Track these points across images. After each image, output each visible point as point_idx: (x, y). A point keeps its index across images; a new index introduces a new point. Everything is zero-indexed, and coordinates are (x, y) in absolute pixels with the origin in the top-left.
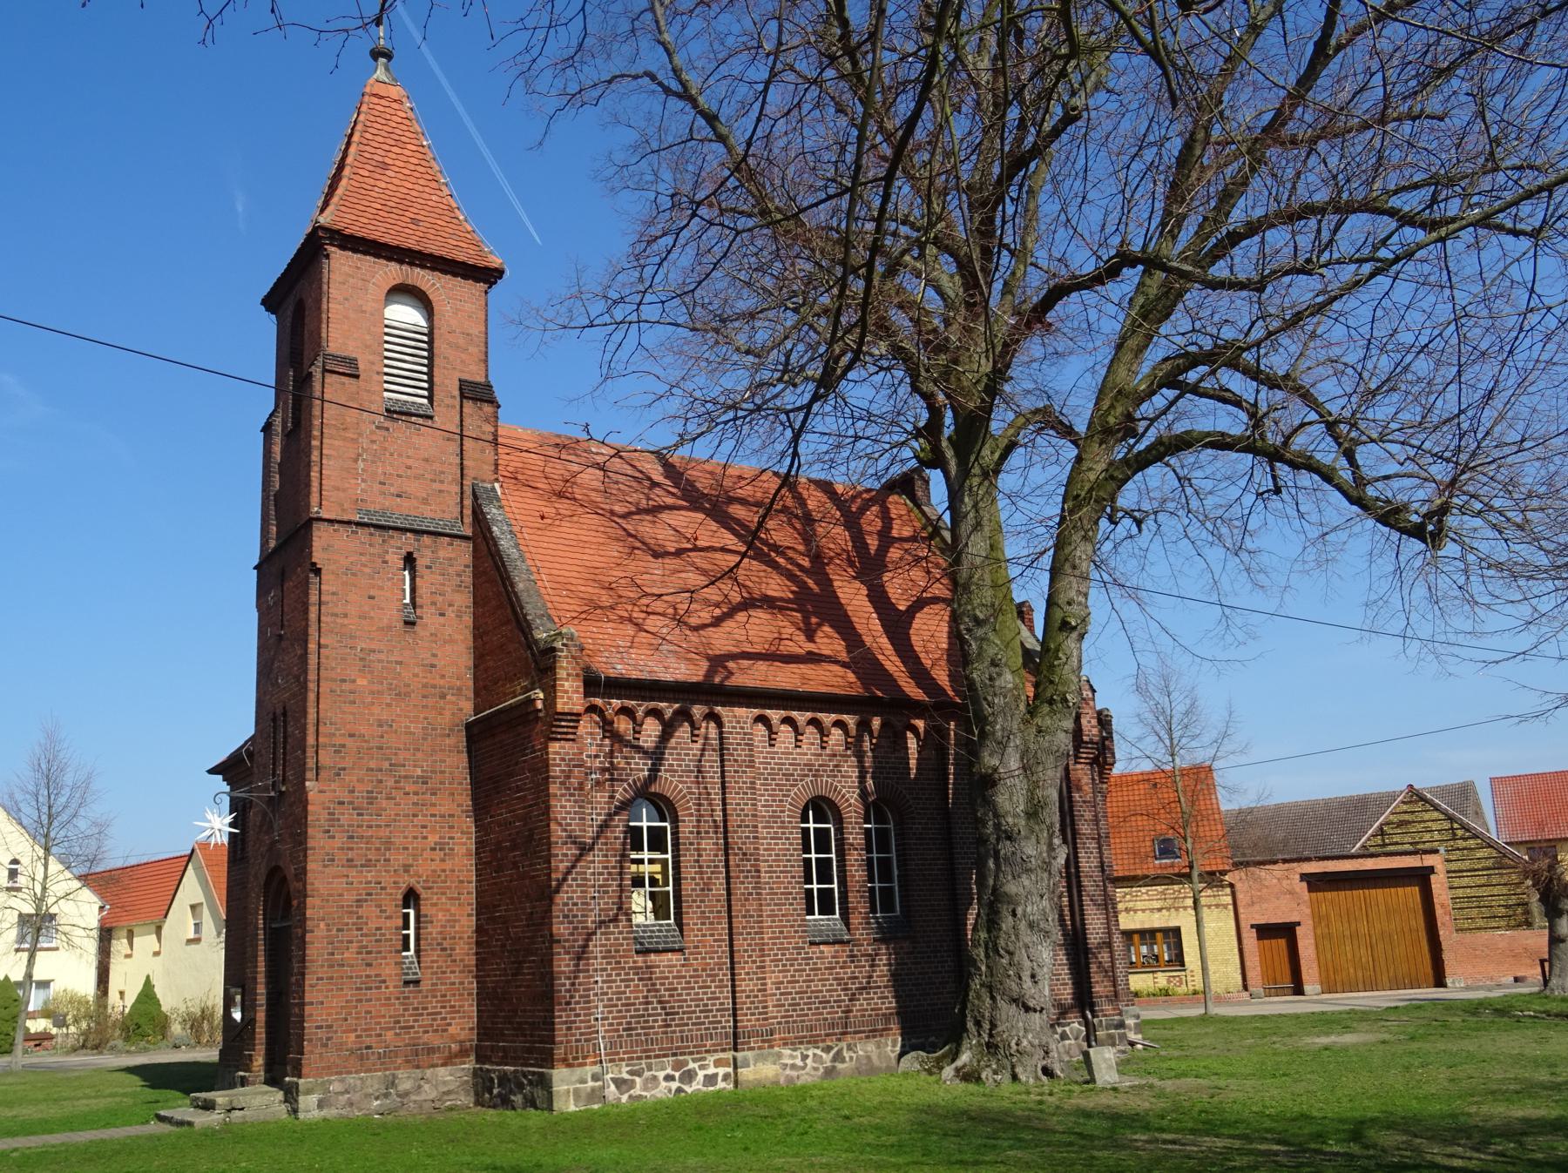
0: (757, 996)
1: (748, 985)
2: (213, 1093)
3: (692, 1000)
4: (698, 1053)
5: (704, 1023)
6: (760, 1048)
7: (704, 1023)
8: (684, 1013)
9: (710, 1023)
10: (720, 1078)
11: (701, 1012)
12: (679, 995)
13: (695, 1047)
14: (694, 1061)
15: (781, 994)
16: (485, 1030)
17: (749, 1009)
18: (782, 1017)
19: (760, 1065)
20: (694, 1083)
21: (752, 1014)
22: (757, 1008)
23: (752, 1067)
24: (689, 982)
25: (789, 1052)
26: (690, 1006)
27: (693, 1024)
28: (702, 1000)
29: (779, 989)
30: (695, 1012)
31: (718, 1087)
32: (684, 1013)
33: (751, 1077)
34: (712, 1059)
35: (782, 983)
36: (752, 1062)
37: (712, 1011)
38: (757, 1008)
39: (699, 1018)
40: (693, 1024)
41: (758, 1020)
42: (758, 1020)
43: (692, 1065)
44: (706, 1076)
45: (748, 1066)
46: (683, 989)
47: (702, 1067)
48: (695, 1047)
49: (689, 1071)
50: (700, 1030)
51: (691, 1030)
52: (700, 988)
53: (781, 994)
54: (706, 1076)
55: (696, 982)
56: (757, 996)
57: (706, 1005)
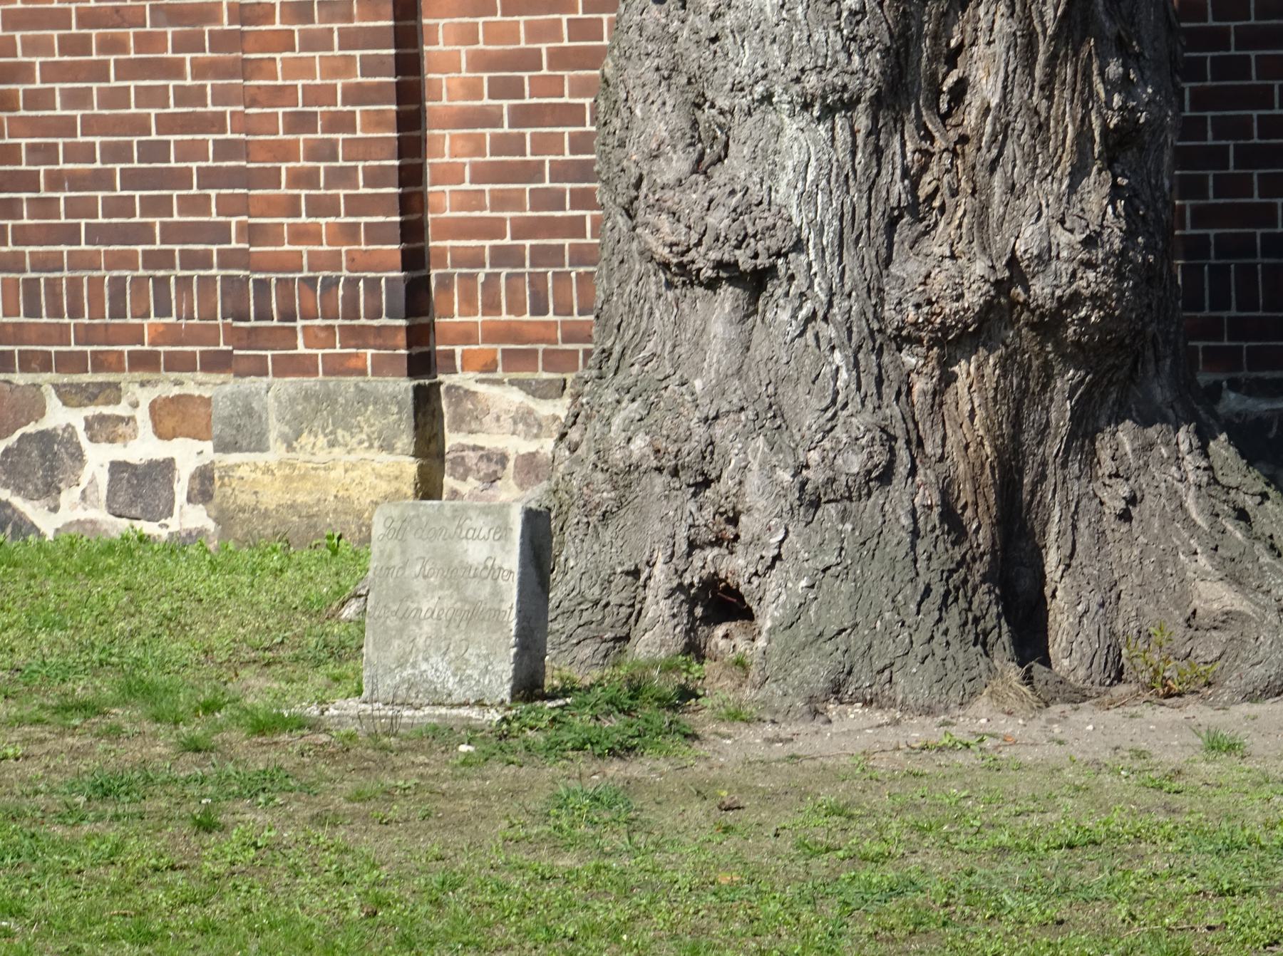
0: (342, 122)
1: (305, 69)
2: (184, 374)
3: (91, 125)
4: (100, 363)
5: (144, 233)
6: (337, 367)
7: (144, 233)
8: (56, 181)
9: (172, 233)
10: (181, 489)
11: (131, 179)
12: (36, 99)
13: (87, 335)
14: (70, 396)
15: (523, 116)
16: (402, 235)
17: (304, 178)
18: (523, 230)
19: (313, 446)
20: (69, 497)
21: (320, 207)
22: (342, 177)
23: (276, 453)
24: (81, 45)
25: (516, 397)
26: (86, 153)
27: (96, 234)
28: (140, 125)
29: (510, 89)
30: (102, 180)
31: (175, 524)
32: (56, 181)
33: (272, 496)
34: (146, 397)
35: (530, 60)
36: (275, 428)
37: (181, 178)
38: (342, 177)
39: (123, 207)
40: (96, 234)
41: (350, 232)
42: (350, 232)
43: (58, 416)
44: (117, 468)
45: (260, 445)
46: (52, 72)
47: (102, 429)
48: (87, 335)
49: (46, 437)
50: (127, 261)
51: (88, 262)
52: (127, 70)
53: (523, 116)
54: (117, 468)
55: (110, 45)
56: (342, 122)
57: (155, 151)
